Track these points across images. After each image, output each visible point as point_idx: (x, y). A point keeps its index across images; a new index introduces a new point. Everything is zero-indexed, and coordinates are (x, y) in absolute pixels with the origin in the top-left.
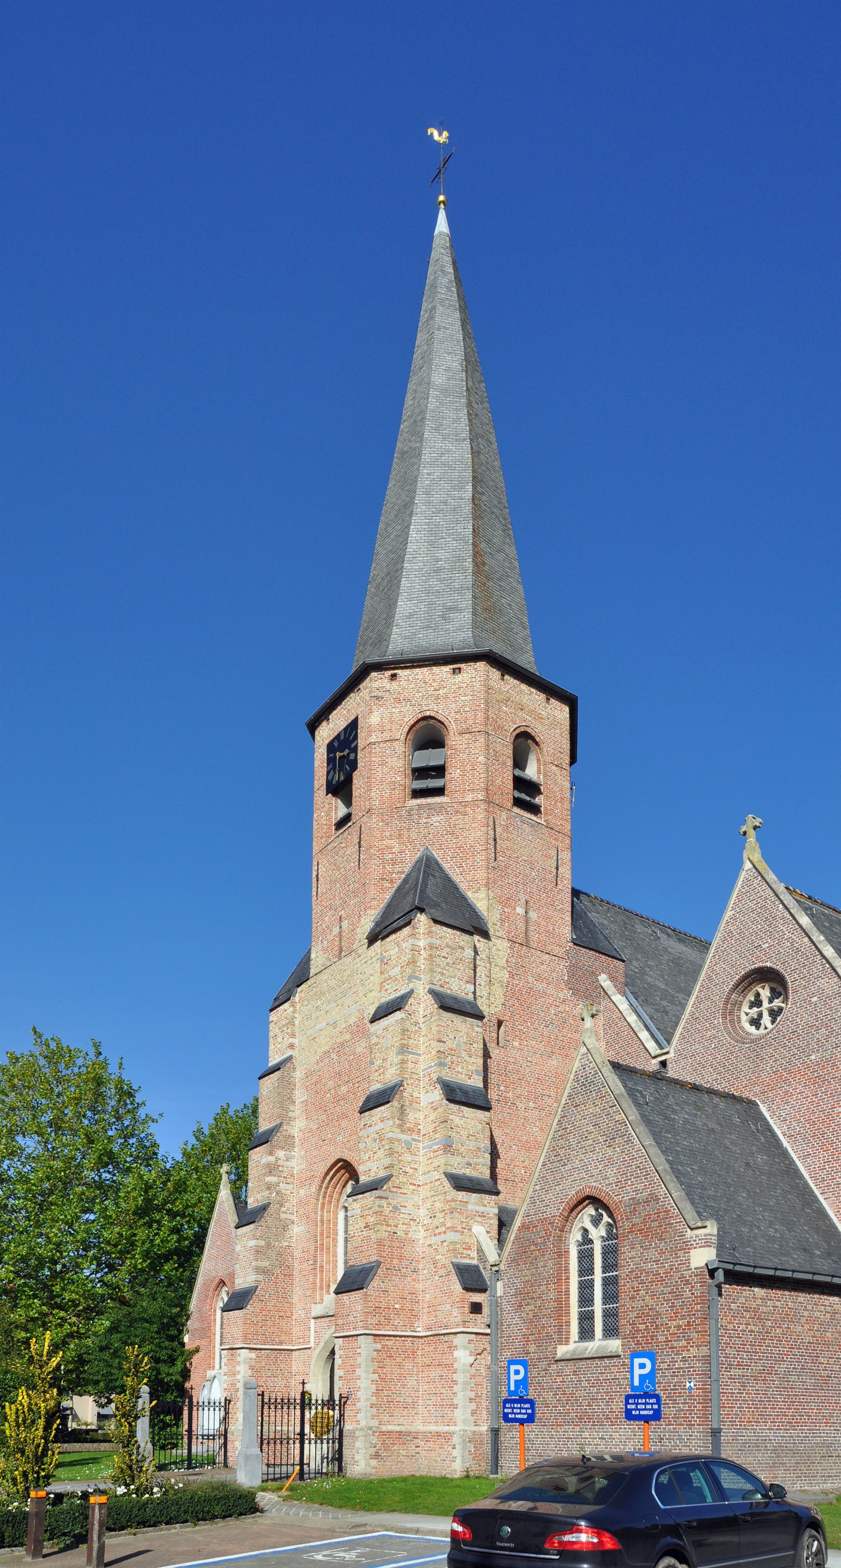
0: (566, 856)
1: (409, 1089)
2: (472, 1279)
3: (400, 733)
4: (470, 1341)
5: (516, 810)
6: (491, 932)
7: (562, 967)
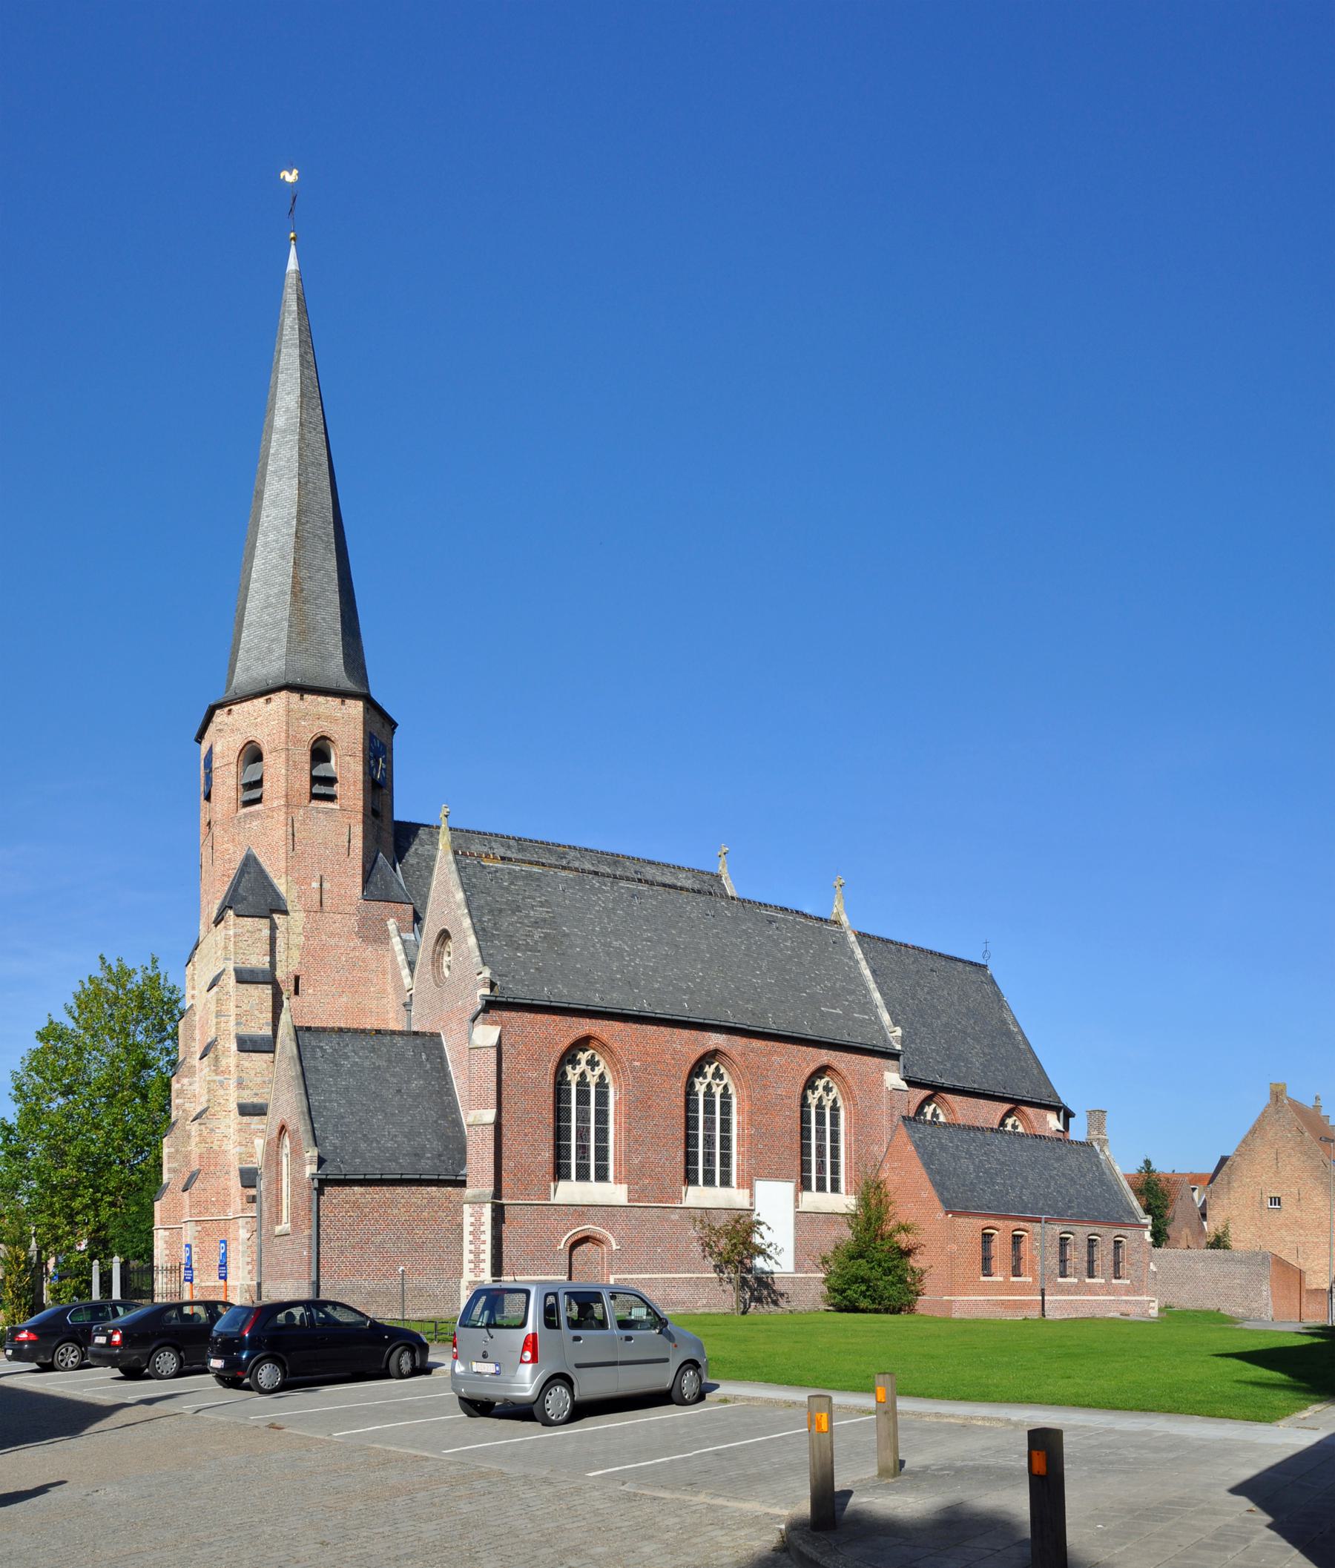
0: (358, 830)
1: (222, 1043)
2: (249, 1178)
3: (233, 757)
5: (315, 803)
6: (289, 908)
7: (353, 922)
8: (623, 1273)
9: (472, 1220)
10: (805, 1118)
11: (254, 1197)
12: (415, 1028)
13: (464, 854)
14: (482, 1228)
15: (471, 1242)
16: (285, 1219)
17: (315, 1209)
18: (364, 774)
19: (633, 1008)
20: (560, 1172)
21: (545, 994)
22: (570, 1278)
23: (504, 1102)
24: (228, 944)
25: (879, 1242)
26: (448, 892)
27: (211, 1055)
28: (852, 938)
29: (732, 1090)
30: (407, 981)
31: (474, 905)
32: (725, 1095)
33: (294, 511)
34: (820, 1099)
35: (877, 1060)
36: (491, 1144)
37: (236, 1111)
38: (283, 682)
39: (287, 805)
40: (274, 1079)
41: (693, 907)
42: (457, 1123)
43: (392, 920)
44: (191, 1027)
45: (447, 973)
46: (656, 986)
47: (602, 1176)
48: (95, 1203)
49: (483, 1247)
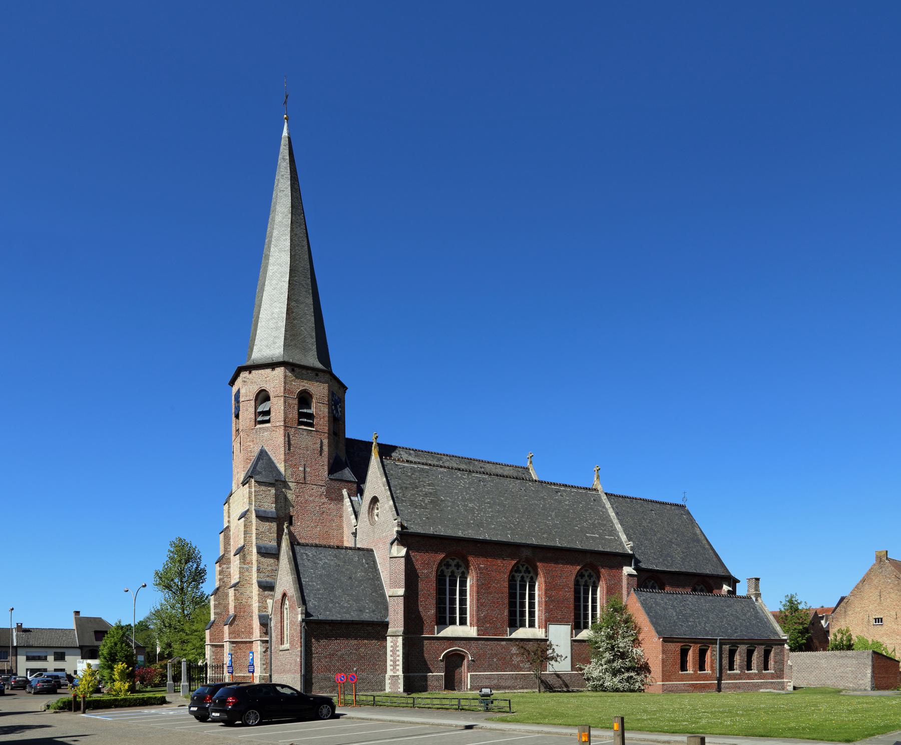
0: (326, 442)
3: (253, 397)
12: (358, 546)
42: (383, 595)
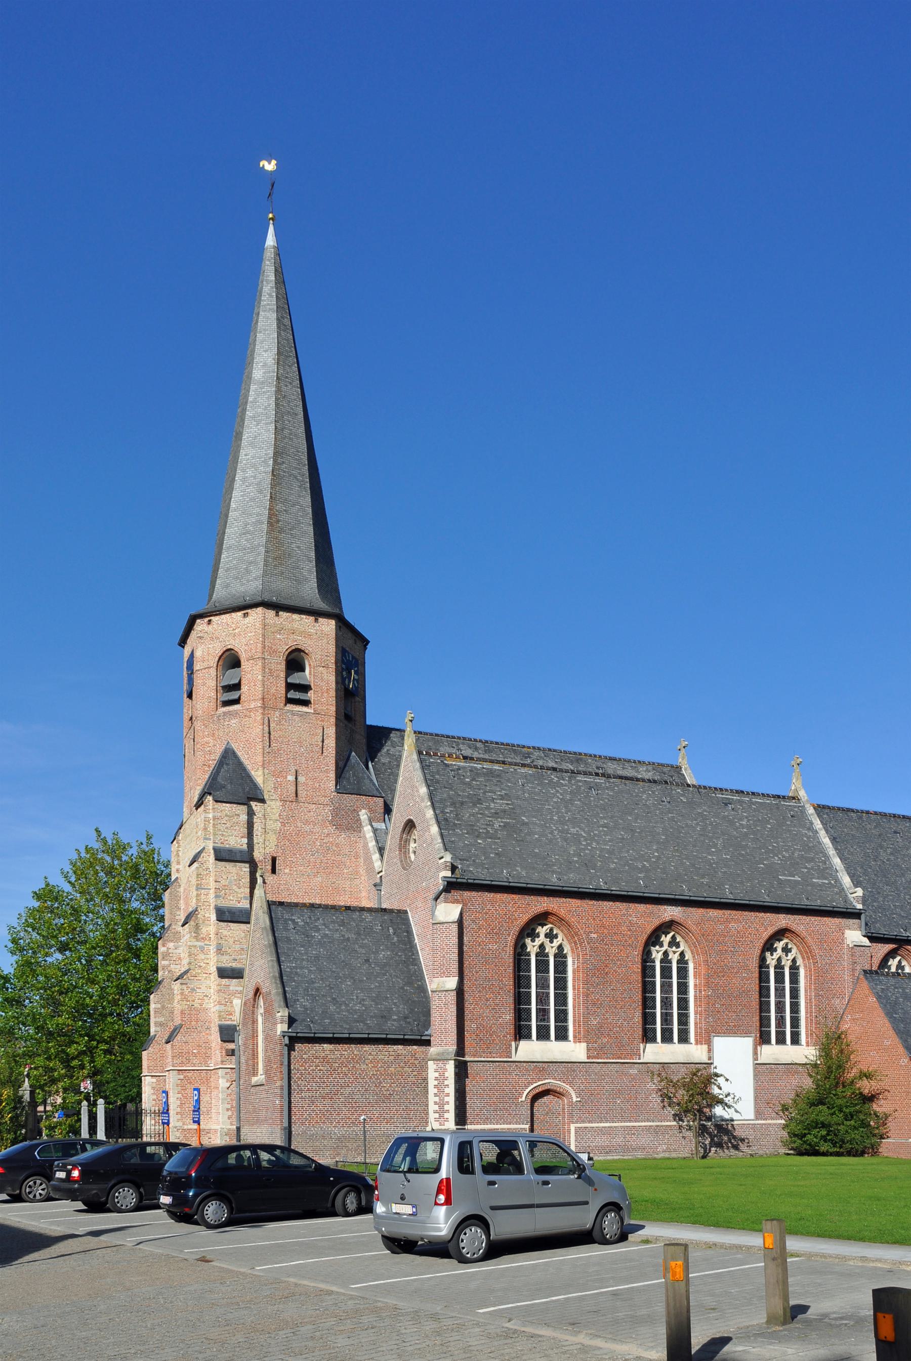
0: (331, 731)
1: (202, 912)
2: (228, 1034)
3: (213, 662)
4: (226, 1074)
5: (290, 707)
6: (266, 797)
7: (327, 812)
8: (583, 1122)
9: (437, 1074)
10: (763, 977)
11: (233, 1051)
12: (384, 906)
13: (428, 754)
14: (446, 1082)
15: (436, 1095)
16: (261, 1071)
17: (286, 1063)
18: (337, 683)
19: (590, 887)
20: (521, 1033)
21: (504, 876)
22: (532, 1130)
23: (466, 972)
24: (208, 826)
25: (840, 1089)
26: (413, 787)
27: (192, 923)
28: (811, 810)
29: (688, 956)
30: (377, 864)
31: (437, 798)
32: (682, 960)
33: (271, 452)
34: (779, 960)
35: (837, 921)
36: (453, 1008)
37: (216, 973)
38: (259, 599)
39: (264, 707)
40: (249, 945)
41: (649, 796)
42: (423, 989)
43: (363, 811)
44: (176, 898)
45: (412, 856)
46: (612, 866)
47: (562, 1035)
48: (90, 1051)
49: (446, 1099)
